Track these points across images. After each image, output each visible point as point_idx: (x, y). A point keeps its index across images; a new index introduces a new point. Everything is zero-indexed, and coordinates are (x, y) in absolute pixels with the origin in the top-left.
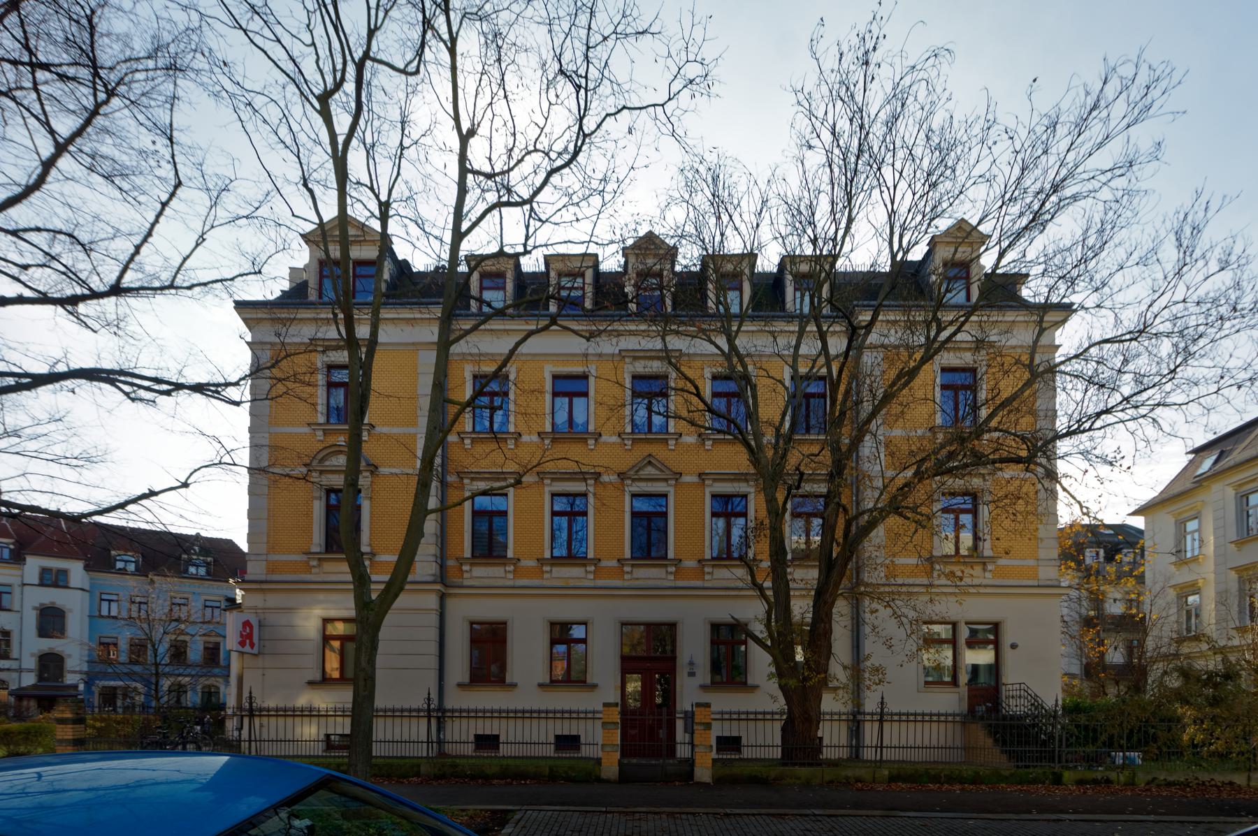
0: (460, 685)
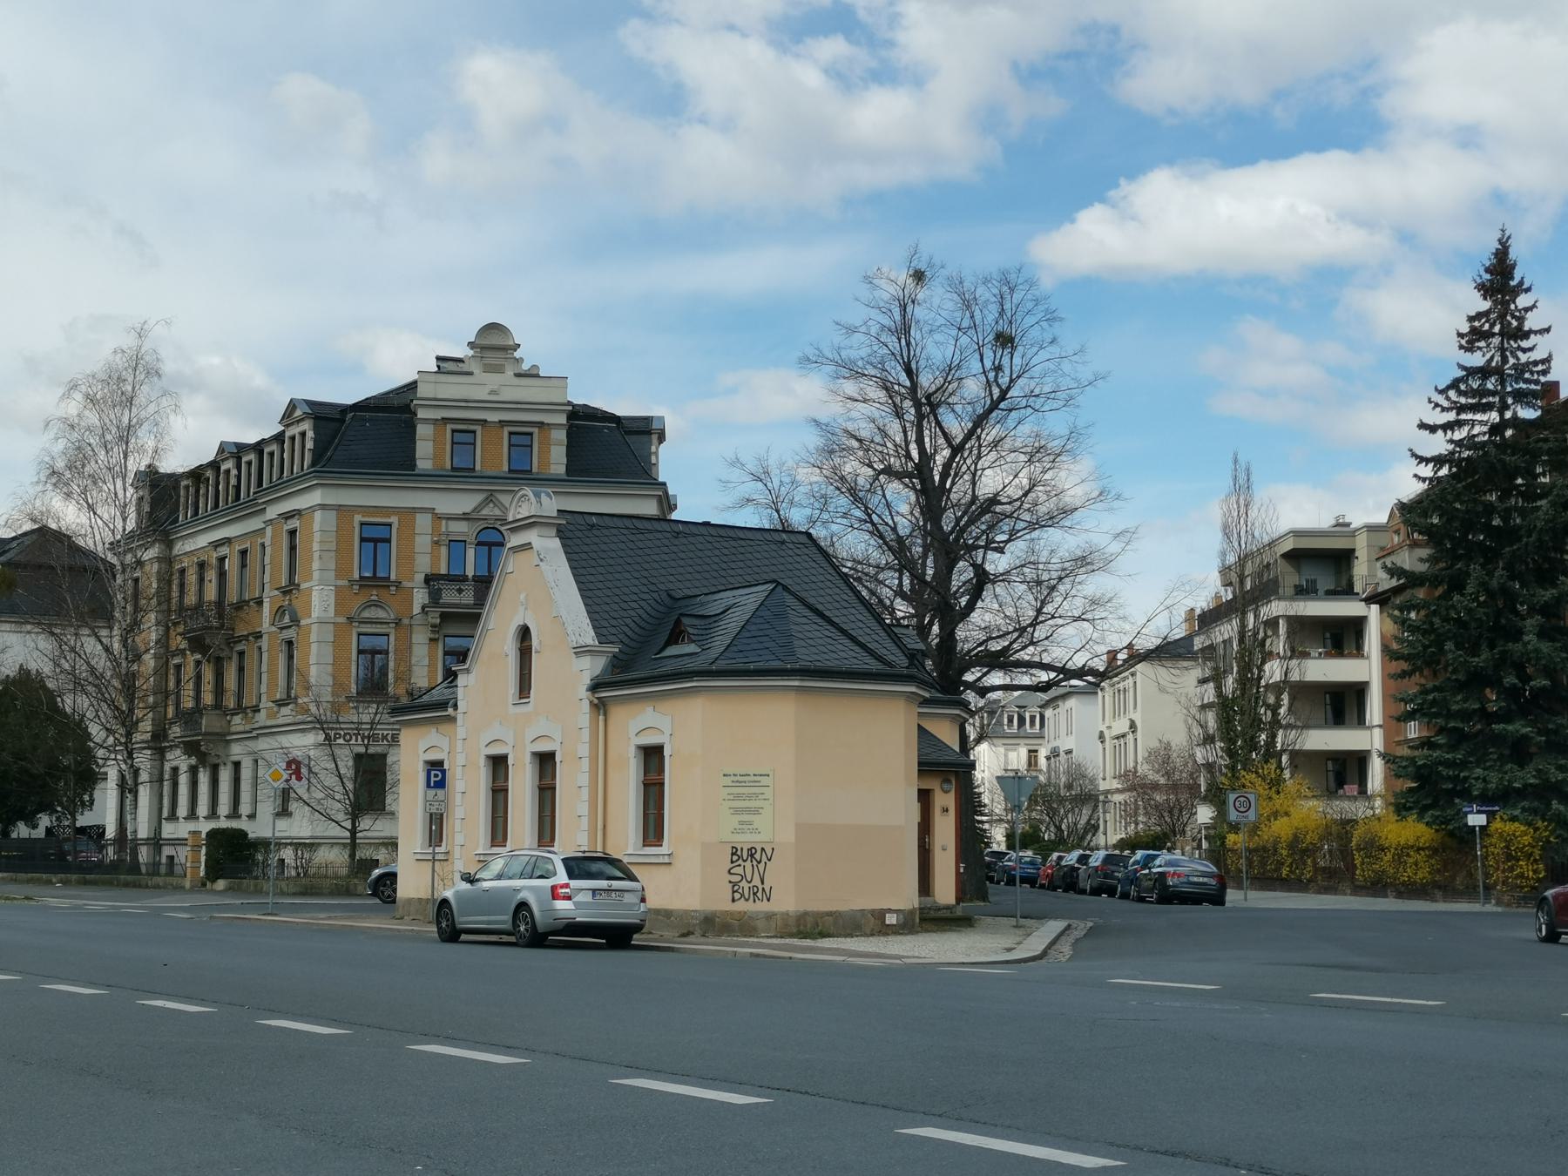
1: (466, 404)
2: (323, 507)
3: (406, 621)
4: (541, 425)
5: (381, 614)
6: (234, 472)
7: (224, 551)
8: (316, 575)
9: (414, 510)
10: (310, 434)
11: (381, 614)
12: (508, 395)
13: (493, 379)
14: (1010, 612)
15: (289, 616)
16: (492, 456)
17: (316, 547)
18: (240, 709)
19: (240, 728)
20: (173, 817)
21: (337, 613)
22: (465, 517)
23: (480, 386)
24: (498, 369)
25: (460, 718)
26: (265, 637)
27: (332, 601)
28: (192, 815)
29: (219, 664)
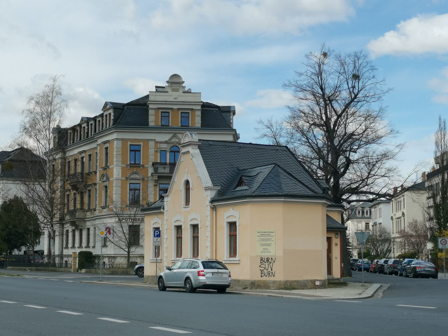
1: (166, 102)
2: (117, 139)
3: (146, 179)
4: (192, 109)
5: (137, 176)
6: (86, 127)
7: (83, 155)
8: (115, 163)
9: (148, 140)
10: (112, 114)
11: (137, 176)
12: (180, 99)
13: (175, 94)
14: (359, 174)
15: (106, 177)
16: (175, 120)
17: (115, 153)
18: (89, 210)
19: (90, 216)
20: (67, 247)
21: (122, 176)
22: (166, 142)
23: (171, 96)
24: (177, 90)
25: (165, 212)
26: (98, 185)
27: (121, 172)
28: (73, 247)
29: (82, 194)
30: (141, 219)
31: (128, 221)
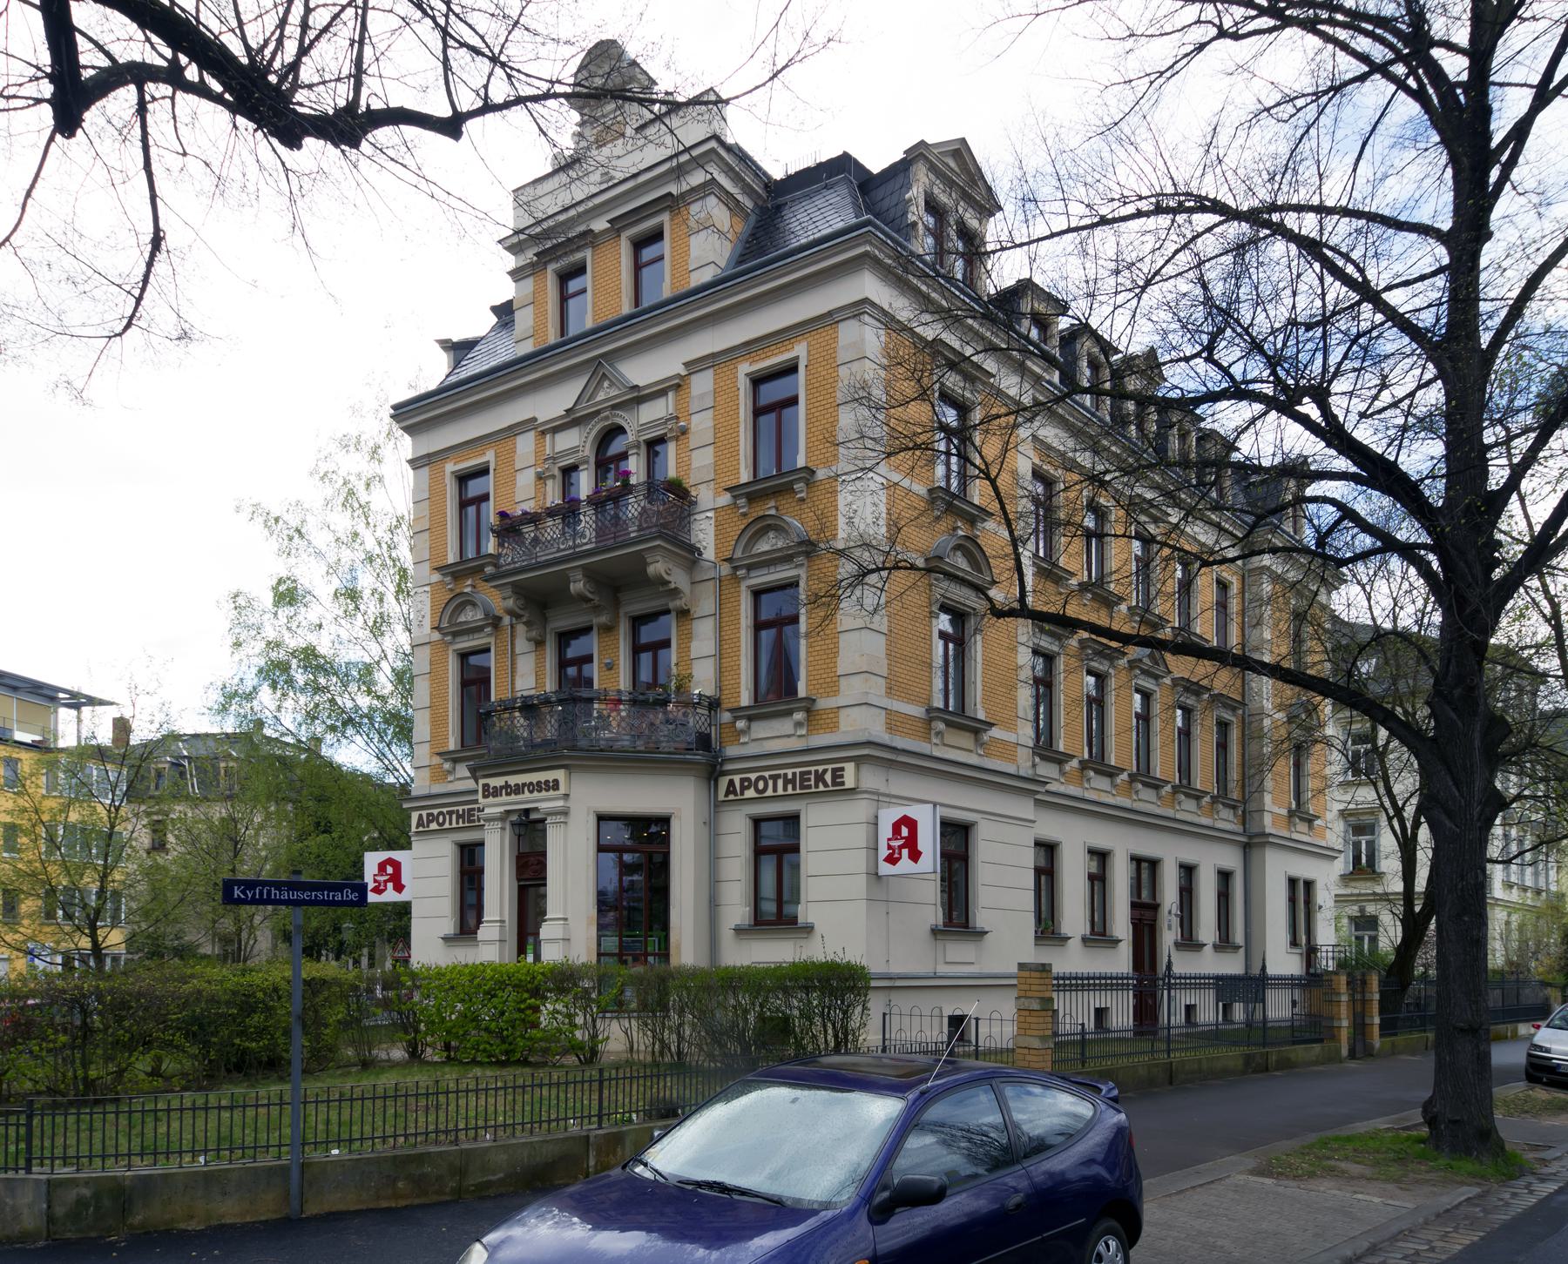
0: (739, 931)
30: (828, 777)
31: (769, 792)
